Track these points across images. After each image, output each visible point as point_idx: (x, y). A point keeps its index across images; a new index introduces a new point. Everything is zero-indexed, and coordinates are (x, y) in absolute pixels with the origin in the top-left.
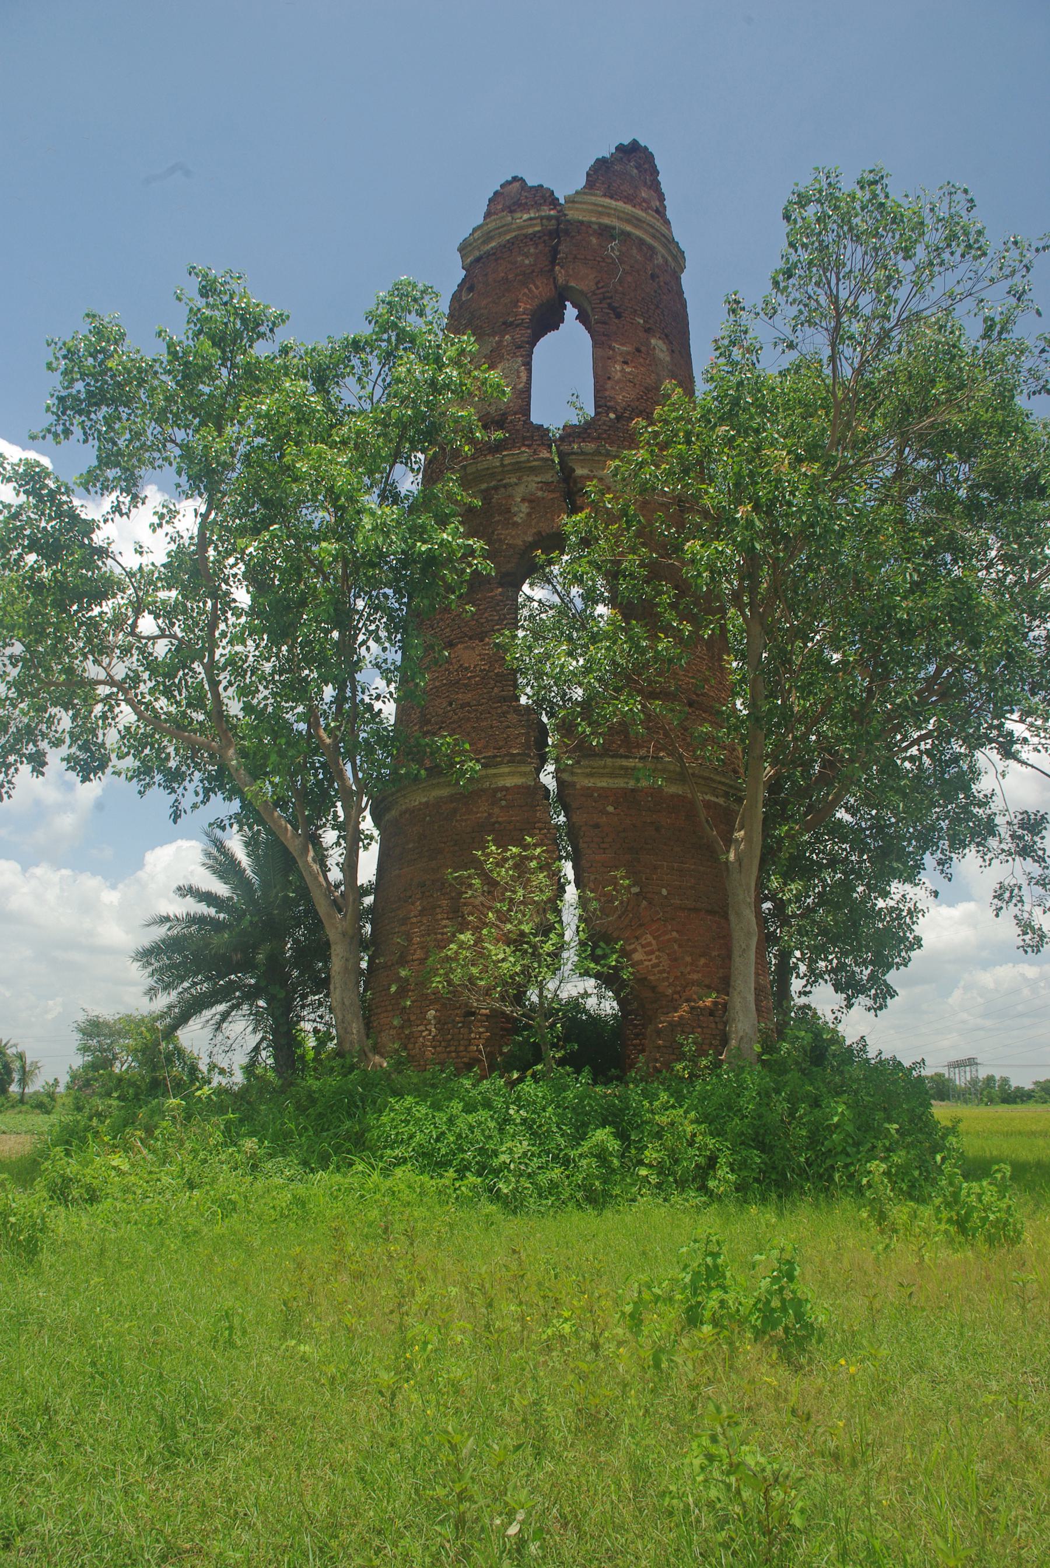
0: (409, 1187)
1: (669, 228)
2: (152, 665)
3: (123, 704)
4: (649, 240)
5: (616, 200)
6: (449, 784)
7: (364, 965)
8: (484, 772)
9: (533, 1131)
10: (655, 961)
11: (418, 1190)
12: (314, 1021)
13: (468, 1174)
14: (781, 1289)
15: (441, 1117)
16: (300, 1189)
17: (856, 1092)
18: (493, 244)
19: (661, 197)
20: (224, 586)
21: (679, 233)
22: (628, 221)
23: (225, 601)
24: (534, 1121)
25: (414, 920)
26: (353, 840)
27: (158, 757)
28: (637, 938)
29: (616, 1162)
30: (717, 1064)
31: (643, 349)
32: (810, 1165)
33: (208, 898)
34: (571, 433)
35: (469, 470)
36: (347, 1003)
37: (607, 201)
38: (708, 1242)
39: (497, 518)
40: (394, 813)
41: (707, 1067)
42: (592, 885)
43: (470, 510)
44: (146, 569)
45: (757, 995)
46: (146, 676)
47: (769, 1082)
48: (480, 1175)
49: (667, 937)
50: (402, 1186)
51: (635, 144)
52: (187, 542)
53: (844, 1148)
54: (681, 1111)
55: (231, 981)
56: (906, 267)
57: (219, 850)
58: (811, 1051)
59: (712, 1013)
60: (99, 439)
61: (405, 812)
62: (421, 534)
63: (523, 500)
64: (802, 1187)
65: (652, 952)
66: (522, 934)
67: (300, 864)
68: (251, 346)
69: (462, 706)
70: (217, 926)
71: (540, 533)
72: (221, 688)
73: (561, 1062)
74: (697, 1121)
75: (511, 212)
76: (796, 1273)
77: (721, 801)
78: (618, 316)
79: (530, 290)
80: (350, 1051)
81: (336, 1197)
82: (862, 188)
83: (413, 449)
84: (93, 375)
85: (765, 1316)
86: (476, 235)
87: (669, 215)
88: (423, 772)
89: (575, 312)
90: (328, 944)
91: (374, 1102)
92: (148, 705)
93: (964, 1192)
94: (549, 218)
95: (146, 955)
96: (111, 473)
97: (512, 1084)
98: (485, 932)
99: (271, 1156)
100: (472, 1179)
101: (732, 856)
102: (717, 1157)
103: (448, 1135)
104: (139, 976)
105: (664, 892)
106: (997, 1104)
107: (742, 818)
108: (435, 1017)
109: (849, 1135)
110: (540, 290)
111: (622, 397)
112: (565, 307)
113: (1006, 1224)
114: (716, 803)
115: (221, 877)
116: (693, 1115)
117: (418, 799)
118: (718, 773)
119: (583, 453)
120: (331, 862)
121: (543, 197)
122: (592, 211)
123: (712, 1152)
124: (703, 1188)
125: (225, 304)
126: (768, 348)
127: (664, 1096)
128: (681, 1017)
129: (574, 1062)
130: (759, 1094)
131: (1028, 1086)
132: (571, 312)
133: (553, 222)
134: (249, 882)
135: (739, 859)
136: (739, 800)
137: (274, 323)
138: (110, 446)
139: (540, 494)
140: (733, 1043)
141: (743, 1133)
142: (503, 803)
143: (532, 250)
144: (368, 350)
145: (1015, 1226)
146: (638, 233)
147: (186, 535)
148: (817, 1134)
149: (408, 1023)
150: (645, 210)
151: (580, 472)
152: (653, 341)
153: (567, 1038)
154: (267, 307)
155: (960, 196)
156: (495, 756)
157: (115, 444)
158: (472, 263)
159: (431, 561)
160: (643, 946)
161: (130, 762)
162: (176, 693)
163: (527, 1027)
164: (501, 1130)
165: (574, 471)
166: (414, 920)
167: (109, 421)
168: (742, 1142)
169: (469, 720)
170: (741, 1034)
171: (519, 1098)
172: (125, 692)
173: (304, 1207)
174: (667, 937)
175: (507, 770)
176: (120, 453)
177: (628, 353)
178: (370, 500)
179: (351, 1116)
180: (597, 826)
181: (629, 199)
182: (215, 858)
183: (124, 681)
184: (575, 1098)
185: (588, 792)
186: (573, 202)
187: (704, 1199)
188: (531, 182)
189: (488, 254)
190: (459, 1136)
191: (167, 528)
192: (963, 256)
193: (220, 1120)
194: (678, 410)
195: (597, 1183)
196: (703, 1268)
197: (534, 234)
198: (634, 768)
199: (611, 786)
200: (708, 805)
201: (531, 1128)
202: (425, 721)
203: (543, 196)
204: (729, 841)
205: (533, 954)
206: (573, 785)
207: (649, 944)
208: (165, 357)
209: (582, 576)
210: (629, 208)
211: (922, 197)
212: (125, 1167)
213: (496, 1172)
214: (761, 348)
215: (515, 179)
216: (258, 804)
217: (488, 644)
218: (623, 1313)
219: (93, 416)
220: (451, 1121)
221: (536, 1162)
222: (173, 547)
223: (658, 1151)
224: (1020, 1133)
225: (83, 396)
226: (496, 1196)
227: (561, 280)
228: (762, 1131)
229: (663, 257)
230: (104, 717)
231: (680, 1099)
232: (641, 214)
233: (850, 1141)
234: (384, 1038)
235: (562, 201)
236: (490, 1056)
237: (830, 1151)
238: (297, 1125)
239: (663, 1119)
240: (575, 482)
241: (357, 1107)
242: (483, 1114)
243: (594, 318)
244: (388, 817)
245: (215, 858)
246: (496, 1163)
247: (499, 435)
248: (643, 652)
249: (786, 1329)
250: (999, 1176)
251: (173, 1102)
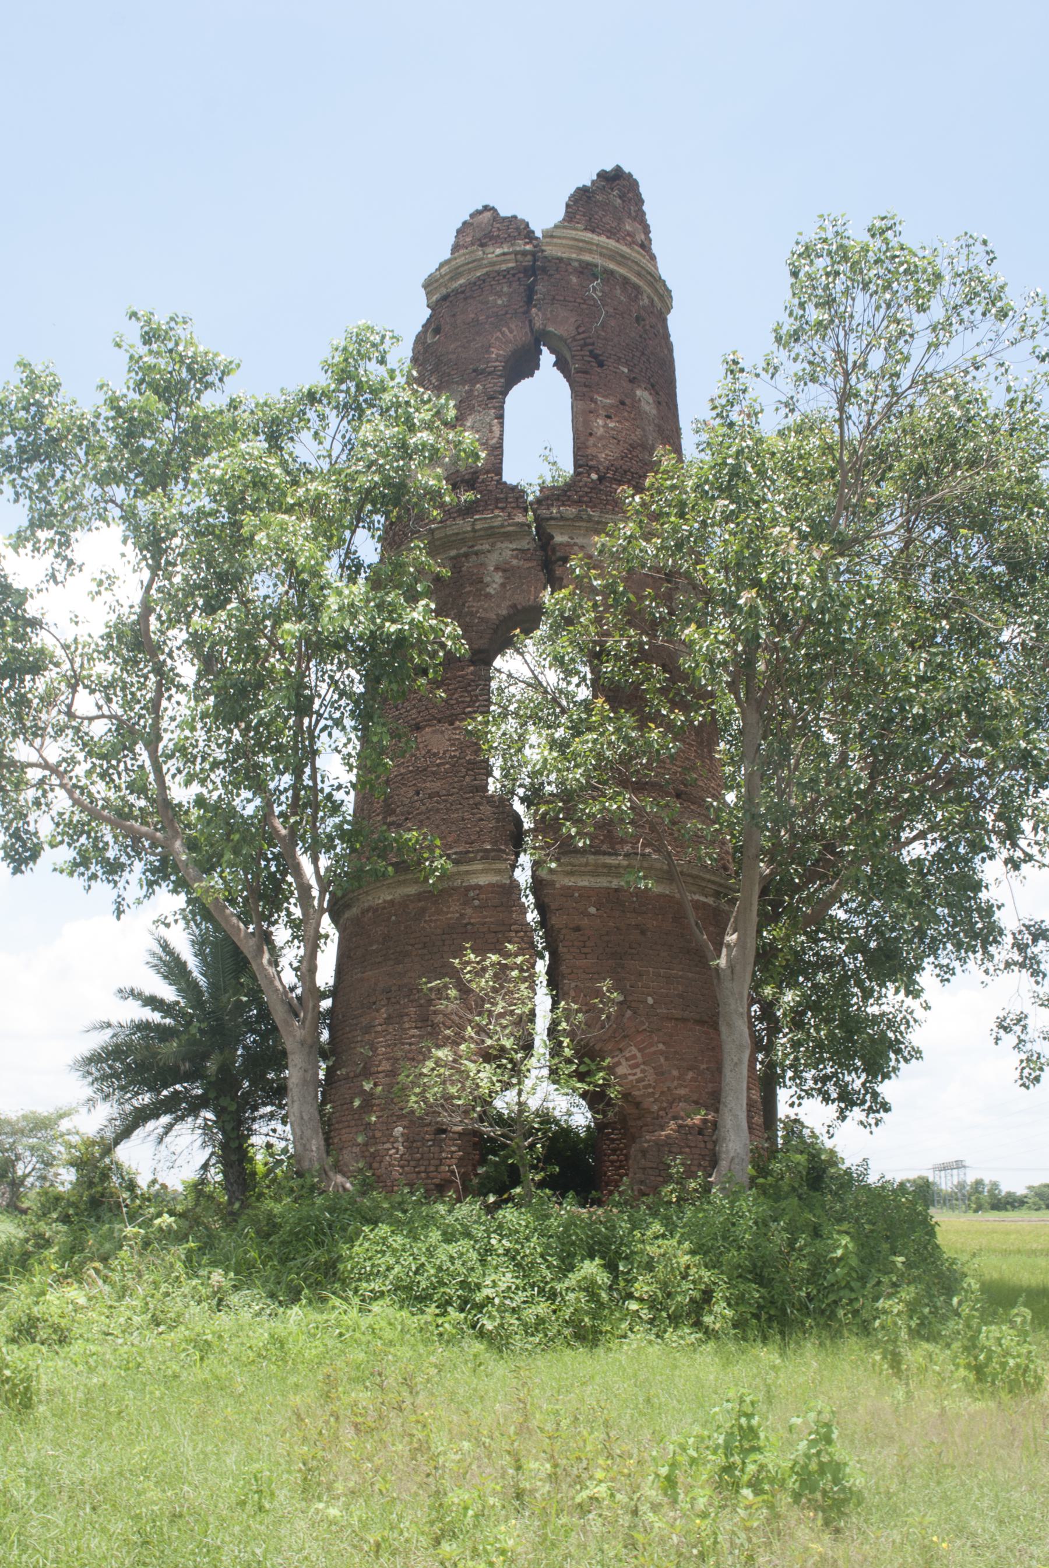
0: (390, 1324)
1: (655, 267)
2: (89, 747)
3: (57, 789)
4: (634, 279)
5: (599, 234)
6: (416, 881)
7: (322, 1075)
8: (455, 870)
9: (522, 1268)
10: (640, 1075)
11: (399, 1327)
12: (267, 1135)
13: (450, 1309)
14: (818, 1454)
15: (419, 1247)
16: (278, 1327)
17: (857, 1220)
18: (462, 281)
19: (646, 229)
20: (169, 661)
21: (667, 269)
22: (612, 258)
23: (166, 679)
24: (517, 1252)
25: (379, 1028)
26: (313, 943)
27: (95, 846)
28: (621, 1050)
29: (604, 1295)
30: (707, 1188)
31: (628, 401)
32: (810, 1301)
33: (153, 1002)
34: (551, 496)
35: (437, 535)
36: (306, 1117)
37: (589, 236)
38: (742, 1401)
39: (468, 589)
40: (355, 911)
41: (696, 1190)
42: (572, 993)
43: (438, 579)
44: (80, 640)
45: (749, 1111)
46: (80, 756)
47: (764, 1209)
48: (462, 1310)
49: (653, 1049)
50: (383, 1324)
51: (618, 170)
52: (126, 610)
53: (848, 1283)
54: (674, 1242)
55: (176, 1092)
56: (921, 322)
57: (164, 950)
58: (808, 1173)
59: (700, 1132)
60: (31, 498)
61: (368, 910)
62: (390, 612)
63: (497, 569)
64: (804, 1324)
65: (637, 1066)
66: (503, 1049)
67: (255, 967)
68: (198, 398)
69: (431, 797)
70: (164, 1033)
71: (514, 606)
72: (168, 778)
73: (541, 1185)
74: (693, 1253)
75: (482, 245)
76: (834, 1436)
77: (710, 901)
78: (601, 365)
79: (503, 333)
80: (309, 1170)
81: (315, 1335)
82: (873, 236)
83: (375, 511)
84: (25, 429)
85: (803, 1480)
86: (443, 271)
87: (655, 248)
88: (390, 869)
89: (553, 358)
90: (284, 1054)
91: (344, 1229)
92: (82, 788)
93: (983, 1335)
94: (524, 253)
95: (94, 1059)
96: (43, 535)
97: (491, 1209)
98: (463, 1047)
99: (236, 1288)
100: (453, 1314)
101: (723, 962)
102: (713, 1291)
103: (428, 1266)
104: (80, 1089)
105: (650, 1001)
106: (986, 1210)
107: (736, 918)
108: (402, 1134)
109: (852, 1268)
110: (514, 334)
111: (605, 455)
112: (540, 352)
113: (1026, 1369)
114: (704, 903)
115: (166, 977)
116: (687, 1245)
117: (383, 896)
118: (708, 871)
119: (562, 518)
120: (284, 962)
121: (517, 229)
122: (571, 247)
123: (707, 1285)
124: (698, 1324)
125: (171, 351)
126: (769, 410)
127: (657, 1227)
128: (668, 1136)
129: (559, 1185)
130: (756, 1223)
131: (1020, 1191)
132: (547, 358)
133: (529, 258)
134: (195, 985)
135: (731, 966)
136: (732, 901)
137: (223, 373)
138: (43, 505)
139: (515, 562)
140: (724, 1164)
141: (739, 1266)
142: (476, 903)
143: (505, 289)
144: (325, 401)
145: (1035, 1371)
146: (622, 271)
147: (126, 604)
148: (820, 1266)
149: (372, 1140)
150: (629, 245)
151: (559, 539)
152: (639, 393)
153: (548, 1158)
154: (216, 355)
155: (979, 248)
156: (468, 852)
157: (48, 503)
158: (437, 301)
159: (401, 642)
160: (627, 1060)
161: (66, 854)
162: (115, 777)
163: (504, 1146)
164: (483, 1261)
165: (552, 537)
166: (379, 1028)
167: (42, 479)
168: (738, 1275)
169: (438, 810)
170: (732, 1154)
171: (500, 1226)
172: (61, 775)
173: (282, 1347)
174: (653, 1049)
175: (480, 867)
176: (52, 514)
177: (612, 406)
178: (331, 569)
179: (319, 1244)
180: (577, 929)
181: (611, 234)
182: (160, 959)
183: (59, 764)
184: (559, 1226)
185: (568, 892)
186: (552, 236)
187: (700, 1335)
188: (504, 212)
189: (457, 292)
190: (440, 1269)
191: (106, 595)
192: (984, 314)
193: (181, 1250)
194: (672, 478)
195: (586, 1319)
196: (736, 1430)
197: (508, 271)
198: (618, 867)
199: (593, 885)
200: (697, 906)
201: (514, 1258)
202: (388, 810)
203: (517, 228)
204: (719, 944)
205: (512, 1070)
206: (552, 883)
207: (634, 1057)
208: (107, 412)
209: (563, 657)
210: (612, 243)
211: (939, 250)
212: (82, 1301)
213: (480, 1307)
214: (762, 411)
215: (486, 208)
216: (209, 901)
217: (459, 728)
218: (657, 1476)
219: (24, 474)
220: (430, 1253)
221: (521, 1296)
222: (113, 617)
223: (649, 1284)
224: (1019, 1252)
225: (13, 451)
226: (481, 1334)
227: (538, 324)
228: (760, 1264)
229: (649, 297)
230: (37, 803)
231: (671, 1228)
232: (625, 249)
233: (854, 1275)
234: (346, 1156)
235: (538, 234)
236: (465, 1178)
237: (833, 1285)
238: (261, 1253)
239: (652, 1250)
240: (554, 550)
241: (325, 1234)
242: (464, 1244)
243: (574, 367)
244: (348, 914)
245: (160, 959)
246: (479, 1297)
247: (468, 496)
248: (629, 742)
249: (825, 1493)
250: (1019, 1320)
251: (130, 1230)
